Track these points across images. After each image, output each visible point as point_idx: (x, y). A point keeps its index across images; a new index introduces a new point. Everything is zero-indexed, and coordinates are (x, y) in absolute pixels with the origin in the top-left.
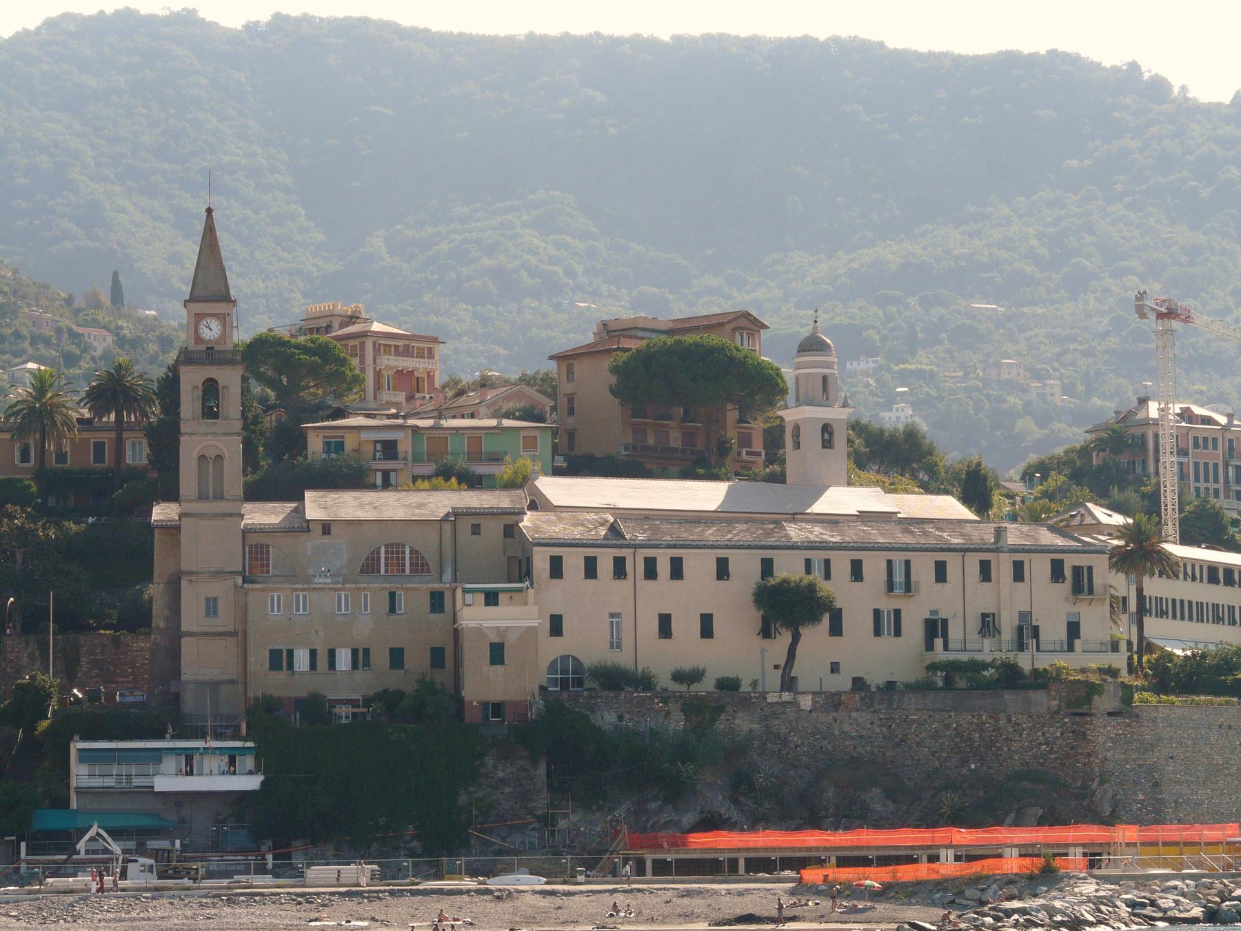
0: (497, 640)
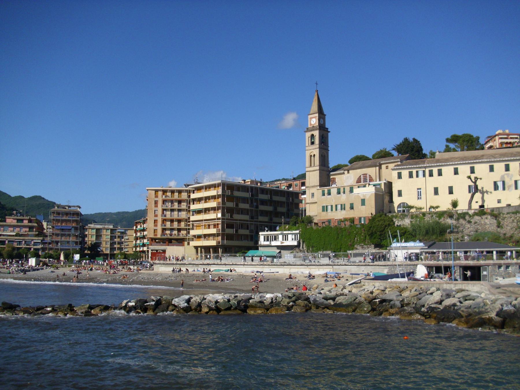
0: (363, 198)
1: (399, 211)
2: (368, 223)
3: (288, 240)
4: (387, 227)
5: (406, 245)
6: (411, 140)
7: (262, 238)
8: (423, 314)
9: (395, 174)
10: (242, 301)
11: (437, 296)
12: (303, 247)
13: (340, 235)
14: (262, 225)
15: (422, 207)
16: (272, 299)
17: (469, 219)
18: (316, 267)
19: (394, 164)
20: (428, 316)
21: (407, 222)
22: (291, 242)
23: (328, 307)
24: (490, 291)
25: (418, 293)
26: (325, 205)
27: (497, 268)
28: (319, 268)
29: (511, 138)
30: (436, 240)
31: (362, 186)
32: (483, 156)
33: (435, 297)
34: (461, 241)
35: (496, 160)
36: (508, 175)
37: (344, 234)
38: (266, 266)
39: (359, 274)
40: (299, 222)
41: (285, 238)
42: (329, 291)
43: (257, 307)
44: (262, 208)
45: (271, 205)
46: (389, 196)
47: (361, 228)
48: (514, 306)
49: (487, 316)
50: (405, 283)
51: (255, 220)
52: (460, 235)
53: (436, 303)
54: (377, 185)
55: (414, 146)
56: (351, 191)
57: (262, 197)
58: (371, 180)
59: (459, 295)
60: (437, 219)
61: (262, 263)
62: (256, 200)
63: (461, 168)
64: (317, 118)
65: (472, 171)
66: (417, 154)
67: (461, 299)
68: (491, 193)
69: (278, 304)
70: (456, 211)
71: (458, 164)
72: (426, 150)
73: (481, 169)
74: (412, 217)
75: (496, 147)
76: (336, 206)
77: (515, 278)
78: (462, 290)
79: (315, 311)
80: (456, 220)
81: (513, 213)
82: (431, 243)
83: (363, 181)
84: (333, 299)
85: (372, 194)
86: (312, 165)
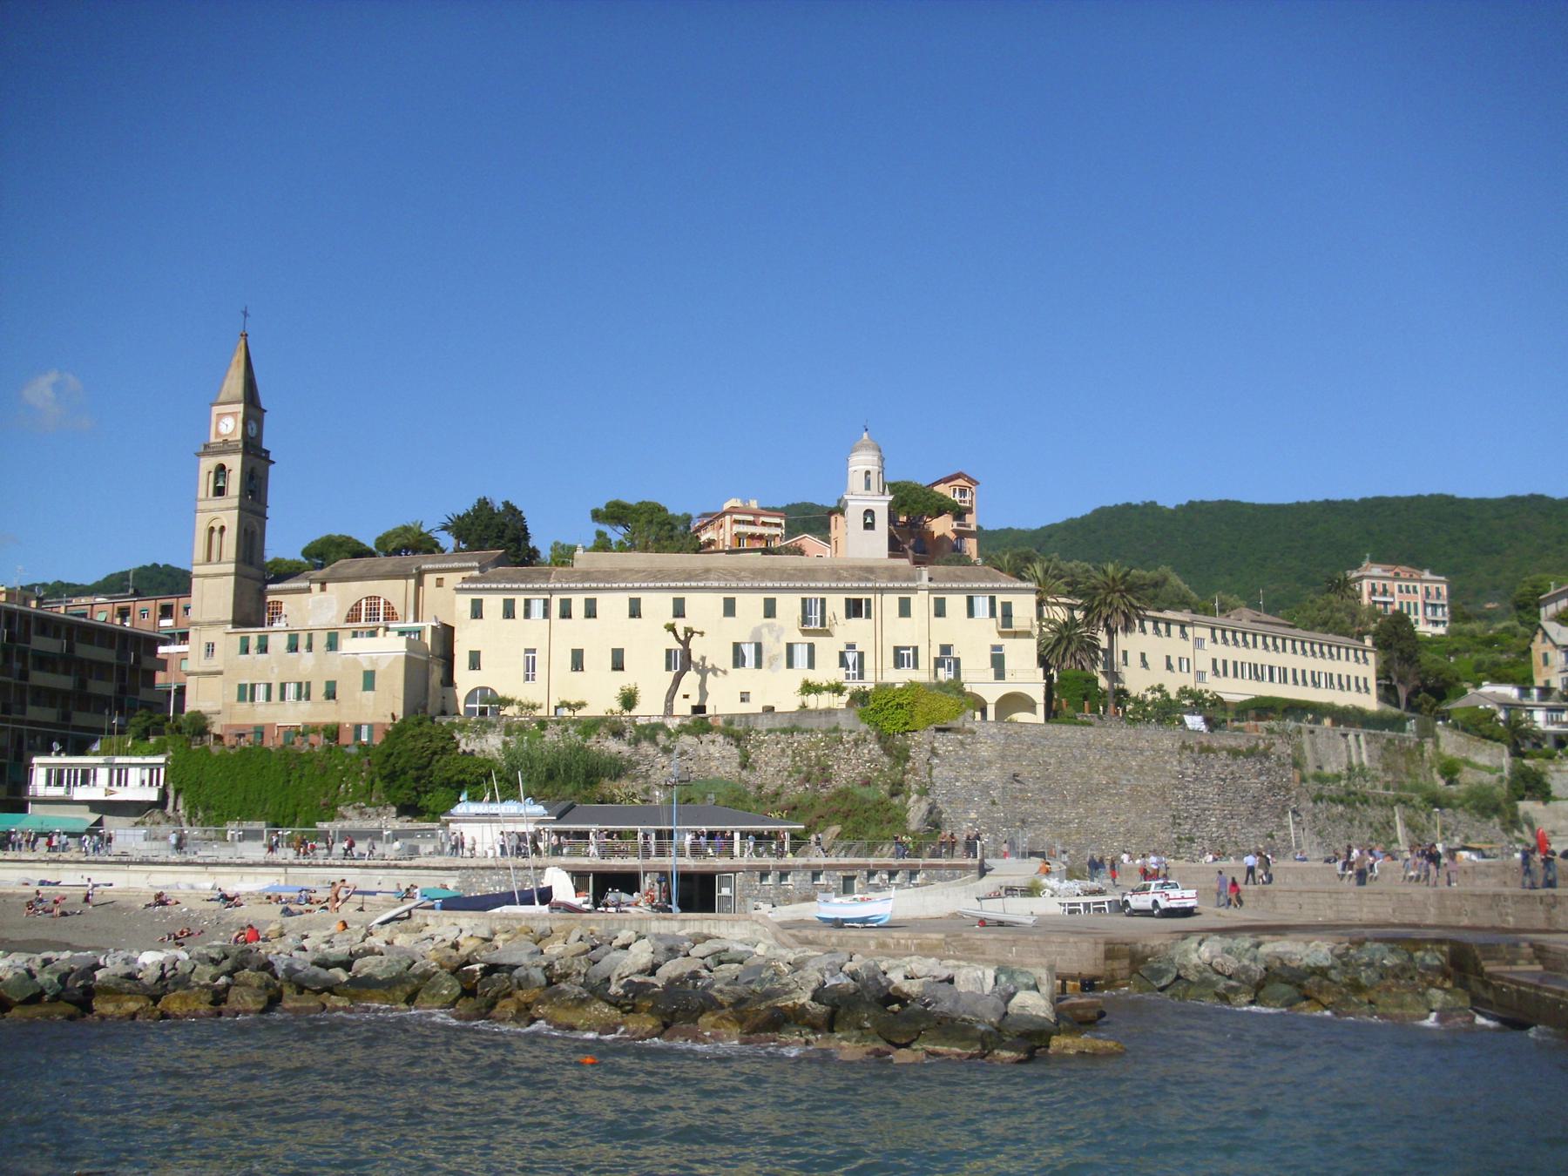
0: (369, 668)
1: (470, 712)
2: (383, 743)
3: (126, 784)
4: (437, 757)
5: (494, 811)
6: (498, 505)
7: (39, 777)
8: (615, 1002)
9: (464, 602)
10: (72, 976)
11: (641, 954)
12: (175, 809)
13: (295, 775)
14: (33, 735)
15: (538, 702)
16: (163, 967)
17: (667, 743)
18: (235, 869)
19: (459, 576)
20: (628, 1008)
21: (492, 744)
22: (138, 788)
23: (331, 988)
24: (777, 939)
25: (588, 946)
26: (248, 682)
27: (758, 879)
28: (242, 874)
29: (764, 524)
30: (575, 799)
31: (365, 631)
32: (707, 571)
33: (636, 956)
34: (644, 801)
35: (741, 585)
36: (771, 628)
37: (306, 771)
38: (66, 866)
39: (374, 893)
40: (167, 731)
41: (119, 776)
42: (328, 942)
43: (121, 993)
44: (39, 678)
45: (67, 672)
46: (444, 665)
47: (358, 757)
48: (853, 976)
49: (790, 1003)
50: (544, 918)
51: (14, 716)
52: (639, 786)
53: (641, 972)
54: (410, 632)
55: (504, 524)
56: (332, 644)
57: (40, 643)
58: (391, 615)
59: (701, 949)
60: (580, 738)
61: (54, 856)
62: (23, 654)
63: (649, 601)
64: (241, 416)
65: (679, 611)
66: (513, 549)
67: (709, 961)
68: (725, 672)
69: (183, 981)
70: (633, 719)
71: (640, 589)
72: (541, 540)
73: (703, 607)
74: (508, 731)
75: (724, 545)
76: (283, 686)
77: (814, 904)
78: (707, 938)
79: (296, 1000)
80: (630, 744)
81: (784, 731)
82: (564, 805)
83: (367, 617)
84: (347, 965)
85: (397, 657)
86: (215, 557)
